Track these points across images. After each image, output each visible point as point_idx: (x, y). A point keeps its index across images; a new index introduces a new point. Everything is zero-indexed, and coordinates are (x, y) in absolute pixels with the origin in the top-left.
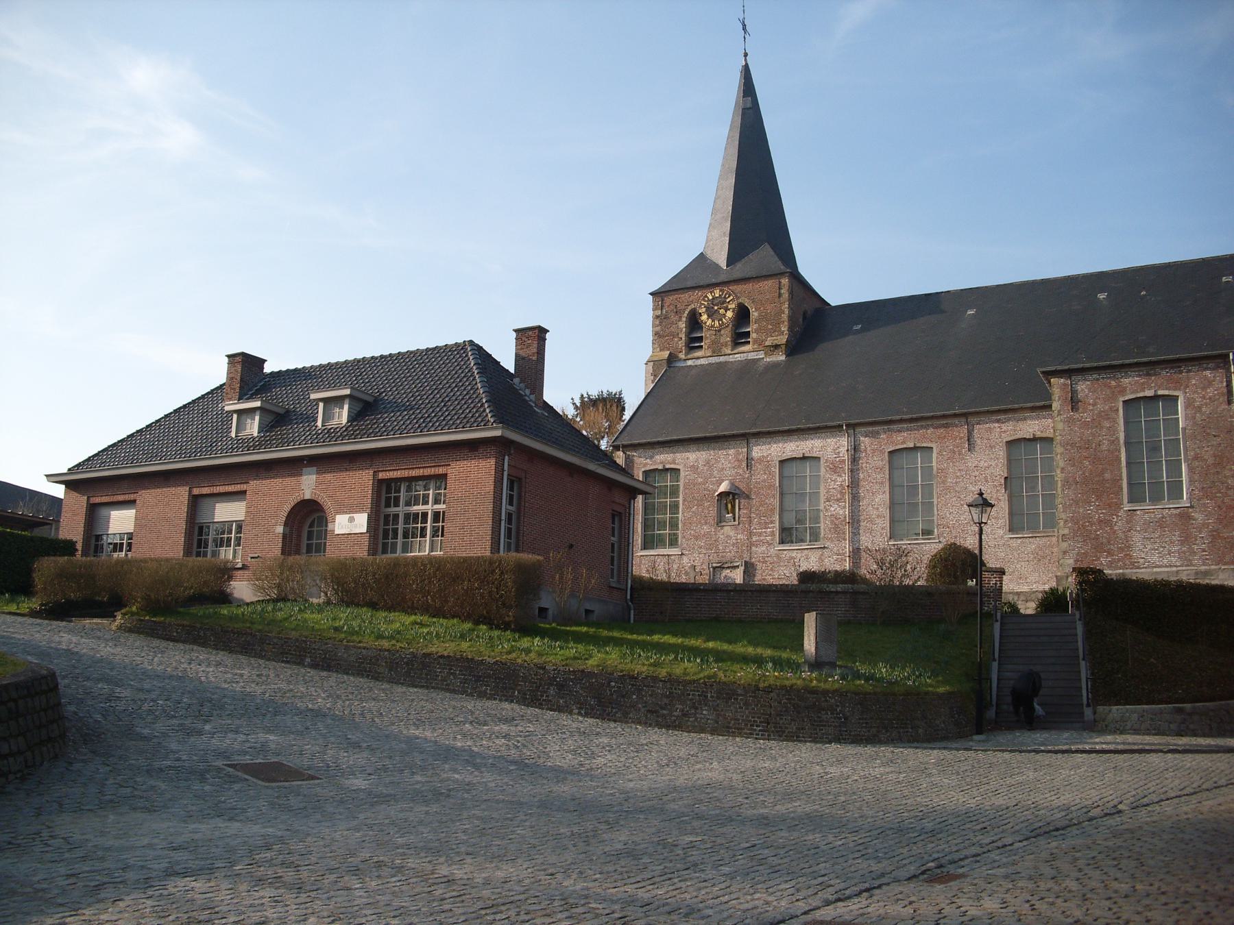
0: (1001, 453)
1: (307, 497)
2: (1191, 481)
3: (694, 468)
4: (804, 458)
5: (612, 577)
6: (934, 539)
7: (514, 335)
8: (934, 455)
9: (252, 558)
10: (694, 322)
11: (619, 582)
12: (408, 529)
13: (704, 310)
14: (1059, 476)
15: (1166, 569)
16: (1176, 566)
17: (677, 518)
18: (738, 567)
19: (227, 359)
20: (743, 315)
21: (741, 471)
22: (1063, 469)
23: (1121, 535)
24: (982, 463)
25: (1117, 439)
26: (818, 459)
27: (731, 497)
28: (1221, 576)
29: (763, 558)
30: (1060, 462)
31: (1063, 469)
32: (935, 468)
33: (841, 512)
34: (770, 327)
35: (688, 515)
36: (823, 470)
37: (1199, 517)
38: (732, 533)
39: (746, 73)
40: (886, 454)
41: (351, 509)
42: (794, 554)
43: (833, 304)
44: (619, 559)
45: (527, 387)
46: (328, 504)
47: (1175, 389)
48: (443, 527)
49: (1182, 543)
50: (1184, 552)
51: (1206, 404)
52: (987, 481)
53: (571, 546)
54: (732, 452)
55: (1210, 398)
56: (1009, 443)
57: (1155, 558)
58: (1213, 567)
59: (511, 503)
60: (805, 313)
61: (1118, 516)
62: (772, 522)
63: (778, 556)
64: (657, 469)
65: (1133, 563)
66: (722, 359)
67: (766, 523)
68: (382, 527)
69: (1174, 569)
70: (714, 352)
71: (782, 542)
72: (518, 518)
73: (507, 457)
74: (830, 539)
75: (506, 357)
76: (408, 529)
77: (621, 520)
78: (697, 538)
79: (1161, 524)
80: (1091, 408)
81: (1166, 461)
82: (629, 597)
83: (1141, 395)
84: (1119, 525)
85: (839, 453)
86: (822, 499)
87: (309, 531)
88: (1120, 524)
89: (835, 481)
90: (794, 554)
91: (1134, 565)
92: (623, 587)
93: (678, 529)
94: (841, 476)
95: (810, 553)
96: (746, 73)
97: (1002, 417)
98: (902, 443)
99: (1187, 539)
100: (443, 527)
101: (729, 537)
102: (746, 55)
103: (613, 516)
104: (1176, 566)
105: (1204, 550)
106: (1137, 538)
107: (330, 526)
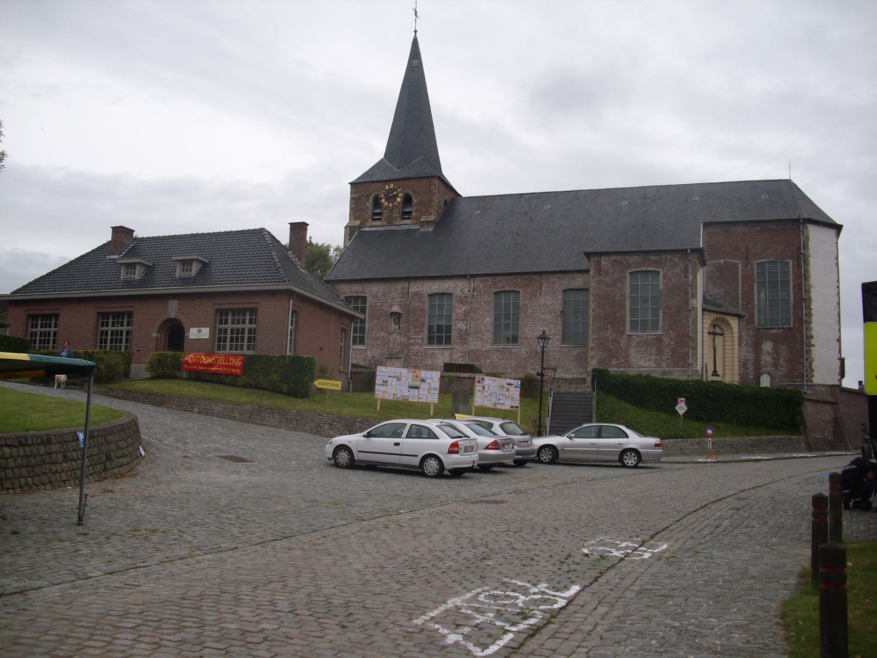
0: (560, 296)
1: (172, 316)
2: (664, 320)
3: (376, 297)
4: (443, 294)
5: (340, 366)
6: (518, 345)
7: (289, 226)
8: (521, 296)
9: (137, 351)
10: (377, 203)
11: (344, 368)
12: (221, 337)
13: (383, 196)
14: (591, 313)
15: (648, 369)
16: (653, 367)
17: (365, 327)
18: (401, 358)
19: (111, 229)
20: (407, 200)
21: (404, 300)
22: (593, 309)
23: (623, 348)
24: (548, 302)
25: (625, 294)
26: (452, 294)
27: (398, 315)
28: (676, 374)
29: (417, 353)
30: (592, 305)
31: (593, 309)
32: (521, 304)
33: (464, 327)
34: (424, 209)
35: (371, 325)
36: (454, 302)
37: (667, 341)
38: (398, 338)
39: (415, 43)
40: (492, 294)
41: (199, 325)
42: (435, 351)
43: (464, 196)
44: (344, 356)
45: (296, 257)
46: (185, 322)
47: (658, 267)
48: (254, 337)
49: (657, 355)
50: (657, 360)
51: (674, 277)
52: (551, 313)
53: (321, 349)
54: (399, 287)
55: (676, 274)
56: (564, 291)
57: (641, 363)
58: (672, 369)
59: (292, 325)
60: (446, 201)
61: (622, 338)
62: (422, 332)
63: (425, 353)
64: (352, 296)
65: (629, 365)
66: (393, 228)
67: (418, 332)
68: (217, 336)
69: (652, 369)
70: (388, 223)
71: (429, 343)
72: (296, 334)
73: (291, 300)
74: (457, 344)
75: (284, 238)
76: (221, 337)
77: (346, 334)
78: (376, 339)
79: (646, 343)
80: (611, 275)
81: (651, 308)
82: (349, 377)
83: (640, 269)
84: (623, 343)
85: (464, 292)
86: (453, 319)
87: (218, 345)
88: (623, 342)
89: (461, 308)
90: (435, 351)
91: (630, 366)
92: (347, 371)
93: (365, 334)
94: (464, 305)
95: (444, 351)
96: (415, 43)
97: (561, 275)
98: (502, 288)
99: (659, 352)
100: (254, 337)
101: (396, 339)
102: (416, 32)
103: (342, 331)
104: (653, 367)
105: (668, 359)
106: (632, 351)
107: (186, 334)
